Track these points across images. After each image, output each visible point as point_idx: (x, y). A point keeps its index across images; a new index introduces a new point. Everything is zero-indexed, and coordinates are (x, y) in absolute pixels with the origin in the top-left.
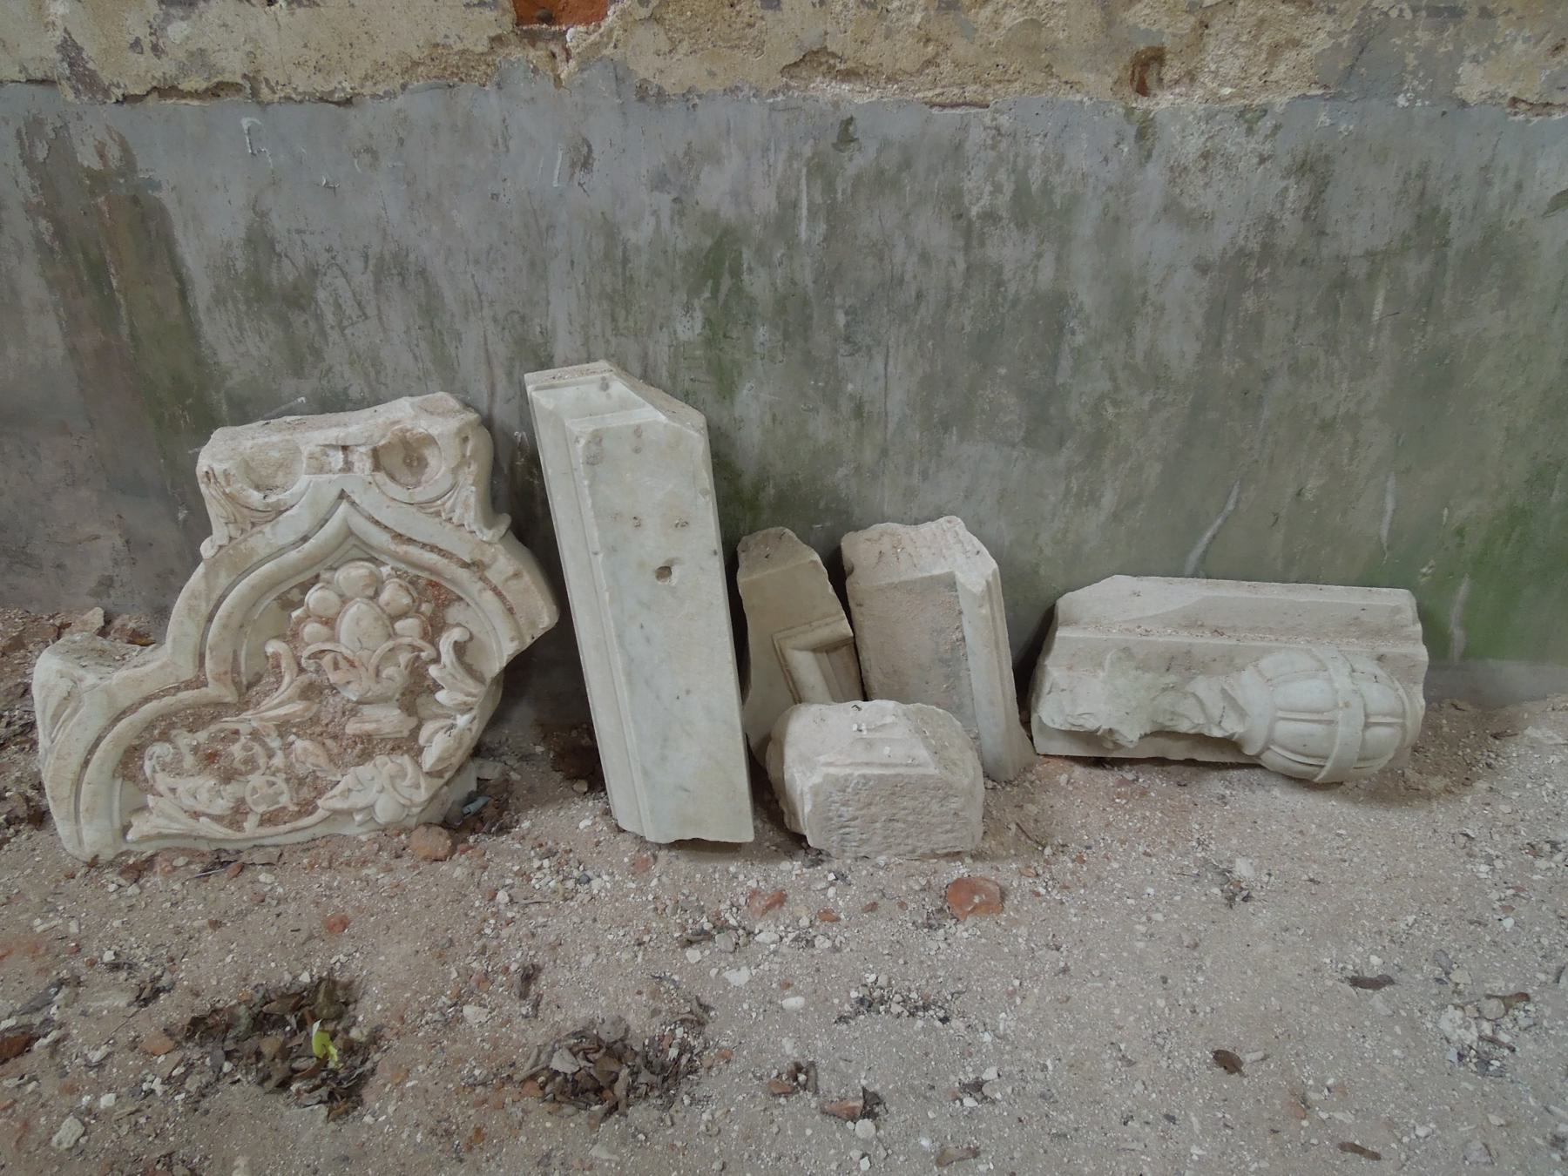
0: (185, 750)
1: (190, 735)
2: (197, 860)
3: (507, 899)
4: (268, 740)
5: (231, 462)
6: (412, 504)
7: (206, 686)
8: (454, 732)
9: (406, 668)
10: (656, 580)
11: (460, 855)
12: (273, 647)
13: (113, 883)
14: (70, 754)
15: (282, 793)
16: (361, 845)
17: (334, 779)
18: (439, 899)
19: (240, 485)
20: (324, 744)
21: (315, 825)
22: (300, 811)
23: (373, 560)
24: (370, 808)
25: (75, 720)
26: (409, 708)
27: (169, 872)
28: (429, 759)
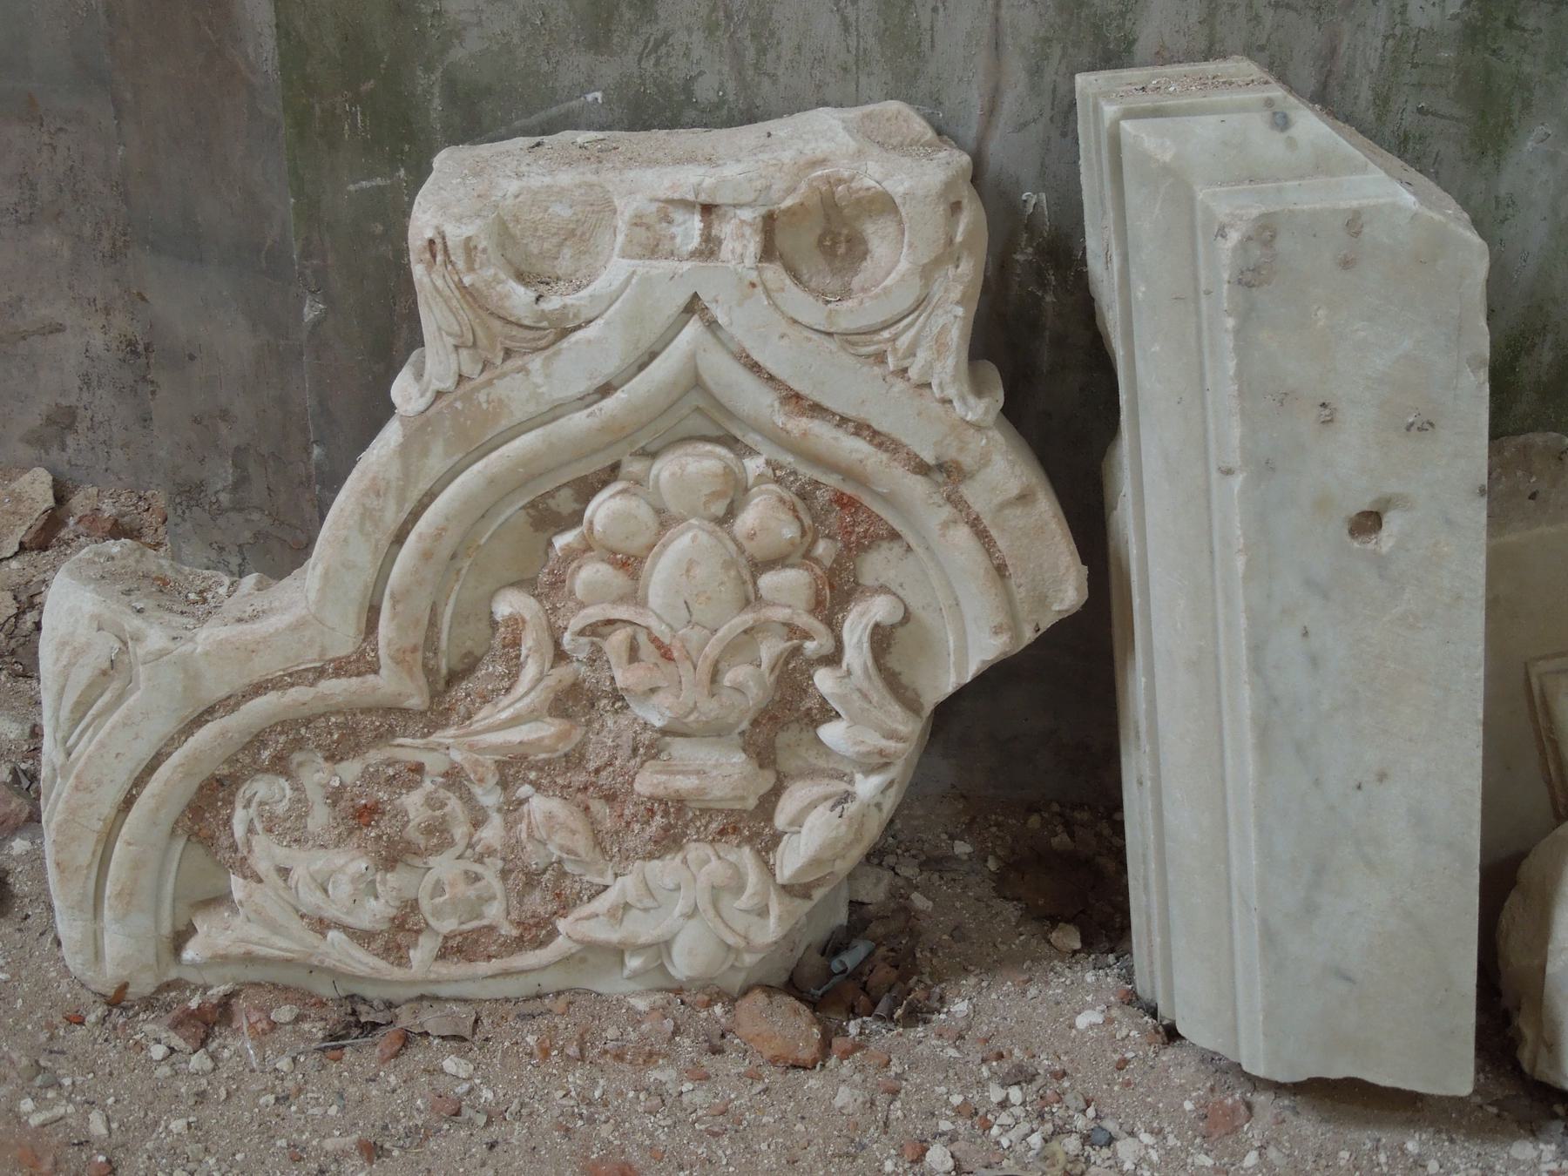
0: (315, 795)
1: (327, 765)
2: (312, 1012)
3: (950, 1163)
4: (477, 790)
5: (478, 222)
6: (830, 334)
7: (376, 672)
8: (851, 808)
9: (772, 670)
10: (1348, 539)
11: (841, 1060)
12: (507, 605)
13: (158, 1041)
14: (99, 783)
15: (493, 898)
16: (636, 1018)
17: (598, 880)
18: (813, 1149)
19: (492, 271)
20: (587, 809)
21: (544, 968)
22: (522, 936)
23: (730, 441)
24: (662, 948)
25: (116, 717)
26: (764, 755)
27: (264, 1033)
28: (792, 859)
